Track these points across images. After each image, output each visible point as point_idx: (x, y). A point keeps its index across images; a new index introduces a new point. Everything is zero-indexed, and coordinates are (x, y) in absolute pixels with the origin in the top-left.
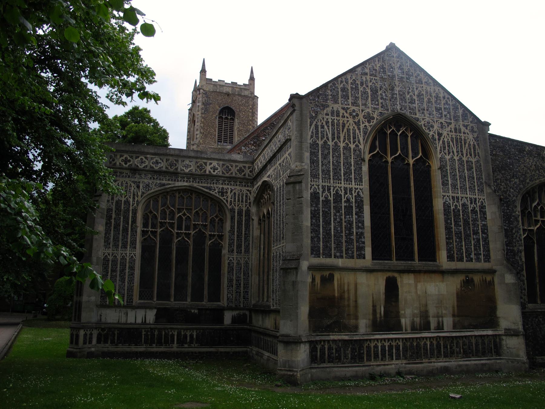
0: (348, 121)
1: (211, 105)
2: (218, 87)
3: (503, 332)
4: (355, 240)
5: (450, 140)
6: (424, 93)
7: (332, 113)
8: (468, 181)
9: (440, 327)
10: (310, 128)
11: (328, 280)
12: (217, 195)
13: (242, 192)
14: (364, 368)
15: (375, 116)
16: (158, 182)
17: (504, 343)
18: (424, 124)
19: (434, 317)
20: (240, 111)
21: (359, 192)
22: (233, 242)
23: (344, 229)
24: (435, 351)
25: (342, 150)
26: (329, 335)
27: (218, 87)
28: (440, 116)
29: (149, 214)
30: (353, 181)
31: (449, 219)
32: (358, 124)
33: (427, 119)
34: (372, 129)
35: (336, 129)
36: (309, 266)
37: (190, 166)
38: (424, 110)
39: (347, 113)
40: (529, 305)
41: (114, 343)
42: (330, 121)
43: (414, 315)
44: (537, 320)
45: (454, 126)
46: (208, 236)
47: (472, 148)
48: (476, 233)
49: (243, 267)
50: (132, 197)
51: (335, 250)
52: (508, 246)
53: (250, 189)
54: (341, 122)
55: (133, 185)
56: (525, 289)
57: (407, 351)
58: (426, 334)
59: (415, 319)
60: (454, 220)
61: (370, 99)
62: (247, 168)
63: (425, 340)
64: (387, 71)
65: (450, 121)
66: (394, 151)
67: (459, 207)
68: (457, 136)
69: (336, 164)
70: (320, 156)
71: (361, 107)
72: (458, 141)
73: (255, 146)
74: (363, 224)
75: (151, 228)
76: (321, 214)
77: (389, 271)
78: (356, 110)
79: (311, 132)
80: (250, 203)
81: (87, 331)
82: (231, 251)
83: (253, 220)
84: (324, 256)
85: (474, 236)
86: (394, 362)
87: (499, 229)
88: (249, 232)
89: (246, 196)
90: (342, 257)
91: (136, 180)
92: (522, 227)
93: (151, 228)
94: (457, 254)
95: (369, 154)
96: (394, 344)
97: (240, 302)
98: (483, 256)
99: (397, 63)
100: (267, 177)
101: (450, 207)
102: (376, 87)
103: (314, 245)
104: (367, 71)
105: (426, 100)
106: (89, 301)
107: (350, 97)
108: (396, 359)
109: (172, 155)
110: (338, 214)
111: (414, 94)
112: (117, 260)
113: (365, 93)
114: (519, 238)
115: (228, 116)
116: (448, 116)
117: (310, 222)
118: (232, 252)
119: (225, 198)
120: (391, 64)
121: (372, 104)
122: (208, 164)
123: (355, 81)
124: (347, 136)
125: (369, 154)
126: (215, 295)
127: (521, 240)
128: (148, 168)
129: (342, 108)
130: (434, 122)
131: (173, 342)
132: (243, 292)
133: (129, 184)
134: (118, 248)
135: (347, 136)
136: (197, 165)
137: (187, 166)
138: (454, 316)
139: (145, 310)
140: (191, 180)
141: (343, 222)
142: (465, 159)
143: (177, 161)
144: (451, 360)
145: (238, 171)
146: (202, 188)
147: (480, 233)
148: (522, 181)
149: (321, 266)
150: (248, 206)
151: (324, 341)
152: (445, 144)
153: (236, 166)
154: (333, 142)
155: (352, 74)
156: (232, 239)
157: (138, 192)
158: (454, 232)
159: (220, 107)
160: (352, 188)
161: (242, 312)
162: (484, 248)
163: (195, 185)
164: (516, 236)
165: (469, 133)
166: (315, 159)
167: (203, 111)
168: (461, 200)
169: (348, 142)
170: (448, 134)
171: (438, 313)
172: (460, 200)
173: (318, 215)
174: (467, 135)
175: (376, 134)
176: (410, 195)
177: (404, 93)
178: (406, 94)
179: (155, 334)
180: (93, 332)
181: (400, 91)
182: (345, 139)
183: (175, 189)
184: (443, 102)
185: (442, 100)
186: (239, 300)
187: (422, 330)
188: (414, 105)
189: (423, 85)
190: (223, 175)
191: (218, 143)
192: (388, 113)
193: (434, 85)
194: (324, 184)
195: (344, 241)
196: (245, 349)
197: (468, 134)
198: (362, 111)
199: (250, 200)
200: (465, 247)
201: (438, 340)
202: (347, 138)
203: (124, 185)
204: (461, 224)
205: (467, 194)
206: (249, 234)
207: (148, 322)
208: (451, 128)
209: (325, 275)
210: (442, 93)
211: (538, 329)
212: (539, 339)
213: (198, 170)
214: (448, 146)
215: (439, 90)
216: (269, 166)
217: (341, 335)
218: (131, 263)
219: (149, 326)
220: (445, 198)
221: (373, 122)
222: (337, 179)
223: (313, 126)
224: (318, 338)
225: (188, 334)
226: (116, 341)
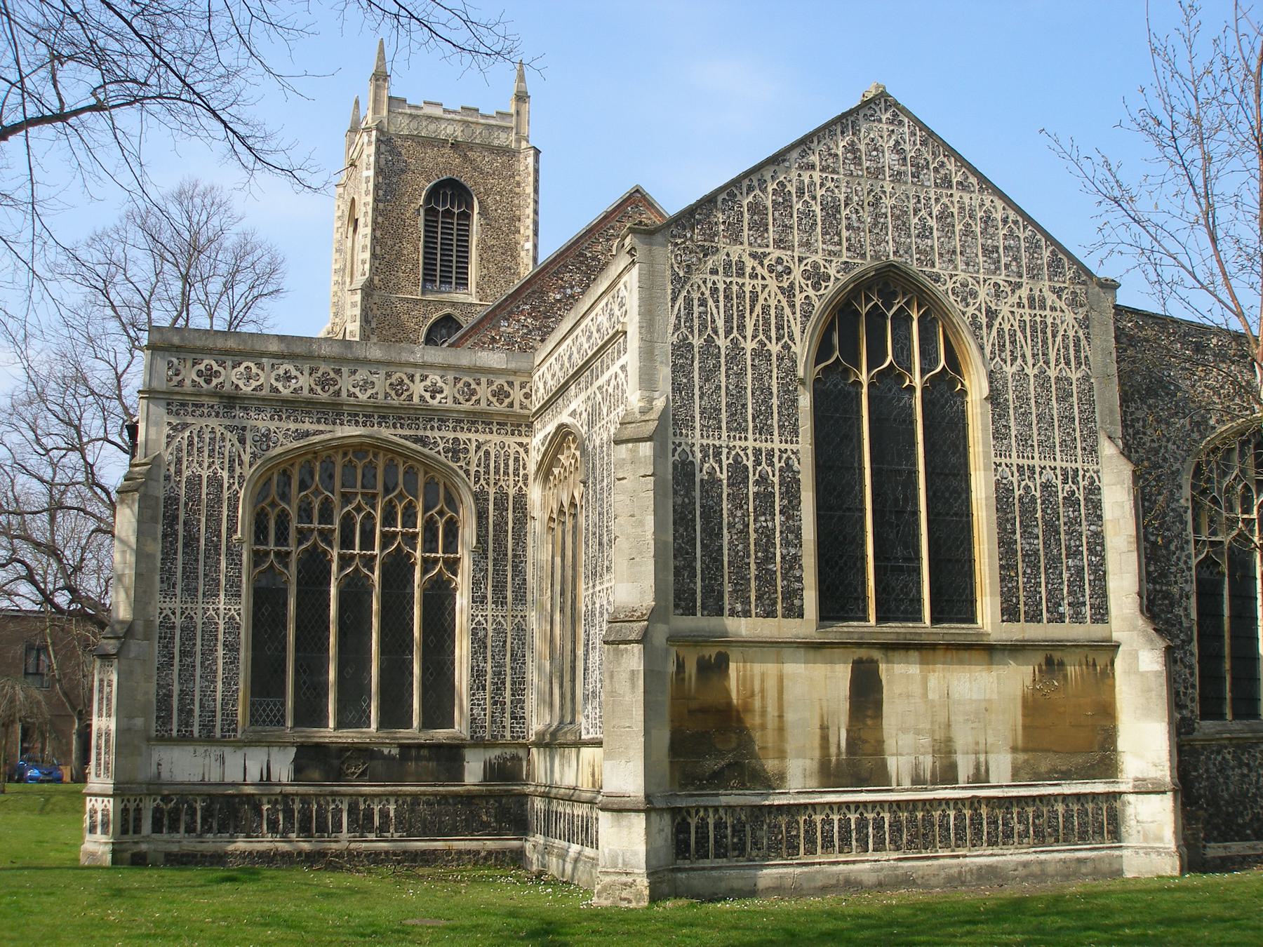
0: (764, 287)
3: (1131, 785)
4: (779, 574)
5: (1016, 327)
6: (955, 211)
7: (728, 265)
8: (1060, 426)
9: (980, 777)
11: (715, 668)
12: (442, 458)
13: (506, 448)
14: (799, 870)
15: (832, 272)
16: (293, 426)
17: (1130, 811)
20: (487, 193)
21: (789, 458)
23: (752, 547)
24: (968, 831)
25: (748, 356)
26: (717, 795)
28: (993, 267)
29: (269, 509)
30: (776, 433)
31: (1007, 520)
32: (789, 292)
33: (962, 276)
35: (735, 308)
36: (671, 636)
38: (954, 252)
39: (762, 266)
40: (1203, 723)
41: (194, 830)
42: (721, 286)
43: (917, 751)
44: (1219, 758)
45: (1028, 292)
47: (1072, 345)
48: (1074, 553)
49: (509, 640)
52: (1158, 583)
54: (748, 289)
55: (228, 435)
56: (1193, 686)
57: (900, 830)
58: (947, 791)
60: (1021, 522)
61: (819, 229)
63: (944, 806)
65: (1018, 280)
66: (876, 356)
67: (1033, 493)
68: (1035, 315)
69: (734, 392)
72: (1039, 331)
73: (535, 318)
74: (798, 536)
75: (276, 545)
76: (698, 513)
77: (859, 645)
78: (785, 258)
79: (674, 317)
80: (526, 477)
81: (128, 801)
82: (478, 600)
85: (1070, 561)
86: (870, 856)
87: (1129, 543)
89: (516, 460)
90: (747, 614)
91: (236, 422)
92: (1192, 535)
93: (276, 545)
94: (1025, 604)
95: (816, 364)
97: (504, 727)
98: (1091, 608)
99: (890, 135)
100: (570, 415)
101: (1013, 490)
102: (834, 198)
103: (682, 586)
104: (815, 159)
105: (959, 227)
106: (129, 729)
107: (771, 228)
110: (739, 513)
111: (930, 214)
112: (195, 627)
114: (1186, 562)
115: (452, 205)
116: (1014, 267)
117: (671, 532)
118: (482, 602)
122: (417, 378)
124: (761, 322)
125: (816, 364)
126: (438, 711)
127: (1190, 569)
128: (265, 392)
129: (750, 255)
130: (978, 282)
133: (219, 435)
134: (196, 596)
135: (761, 322)
138: (1014, 749)
139: (266, 749)
141: (751, 531)
142: (1052, 373)
146: (403, 441)
147: (1085, 553)
148: (1198, 424)
149: (699, 636)
150: (521, 484)
151: (706, 808)
152: (1003, 337)
154: (729, 340)
155: (776, 168)
157: (242, 453)
158: (1019, 553)
160: (773, 450)
161: (509, 752)
162: (1094, 590)
164: (1179, 559)
165: (1064, 307)
166: (685, 380)
167: (381, 193)
168: (1041, 473)
169: (764, 339)
170: (1012, 313)
172: (1037, 476)
174: (1061, 314)
175: (832, 322)
176: (915, 464)
179: (293, 809)
180: (141, 805)
181: (895, 207)
182: (756, 330)
183: (334, 443)
184: (1002, 233)
185: (1000, 226)
188: (929, 242)
189: (954, 191)
191: (424, 286)
192: (865, 264)
193: (981, 190)
194: (705, 442)
195: (752, 576)
197: (1063, 311)
199: (524, 469)
200: (1046, 586)
201: (976, 805)
202: (761, 328)
203: (207, 437)
204: (1039, 531)
205: (1055, 459)
207: (274, 779)
208: (1020, 297)
209: (707, 657)
210: (1000, 208)
211: (1221, 780)
212: (1222, 803)
214: (1010, 342)
215: (992, 201)
216: (573, 387)
217: (745, 795)
219: (278, 789)
220: (1000, 469)
221: (826, 287)
222: (736, 429)
223: (680, 301)
224: (692, 802)
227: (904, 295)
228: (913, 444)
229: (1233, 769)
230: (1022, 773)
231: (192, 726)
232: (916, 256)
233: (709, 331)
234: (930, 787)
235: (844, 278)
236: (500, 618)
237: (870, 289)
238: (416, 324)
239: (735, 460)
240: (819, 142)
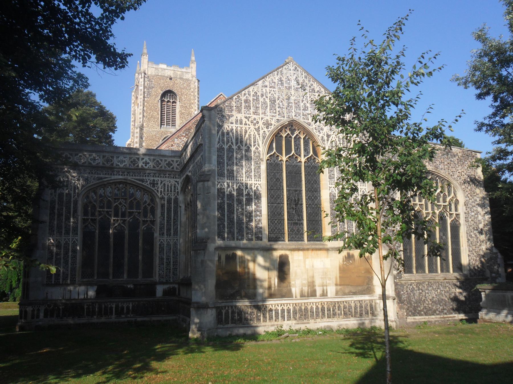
0: (249, 128)
1: (153, 89)
2: (160, 70)
7: (237, 121)
9: (324, 294)
10: (217, 135)
12: (149, 186)
15: (273, 122)
16: (96, 176)
18: (315, 128)
19: (319, 286)
20: (182, 95)
21: (257, 186)
22: (164, 227)
26: (232, 302)
27: (160, 70)
32: (258, 130)
34: (270, 134)
37: (125, 161)
40: (405, 275)
43: (303, 285)
44: (411, 287)
46: (141, 222)
50: (73, 190)
51: (237, 234)
53: (178, 180)
54: (244, 129)
57: (296, 313)
59: (304, 288)
62: (175, 162)
64: (284, 83)
66: (288, 151)
70: (225, 158)
71: (261, 116)
78: (256, 118)
80: (178, 192)
83: (180, 207)
84: (228, 239)
88: (177, 217)
89: (175, 187)
93: (91, 216)
96: (286, 308)
104: (267, 83)
108: (288, 320)
109: (108, 152)
110: (240, 205)
111: (308, 102)
112: (61, 245)
113: (265, 103)
118: (163, 235)
119: (156, 188)
120: (288, 77)
121: (270, 113)
123: (257, 93)
126: (149, 271)
131: (111, 313)
132: (173, 269)
136: (131, 160)
137: (122, 162)
138: (336, 285)
140: (126, 174)
143: (113, 157)
144: (333, 320)
145: (167, 164)
146: (135, 181)
150: (176, 195)
153: (166, 161)
155: (254, 87)
156: (162, 224)
159: (162, 91)
160: (252, 184)
161: (171, 286)
163: (129, 178)
166: (222, 161)
171: (323, 283)
173: (223, 207)
177: (299, 101)
178: (301, 102)
183: (111, 182)
186: (169, 276)
187: (309, 297)
190: (154, 169)
192: (285, 120)
196: (174, 317)
198: (262, 119)
199: (177, 189)
201: (323, 304)
206: (178, 219)
211: (412, 295)
213: (132, 165)
218: (74, 247)
224: (223, 304)
225: (125, 306)
226: (61, 315)
227: (298, 130)
228: (301, 181)
229: (416, 291)
230: (339, 293)
231: (59, 279)
232: (302, 117)
233: (230, 143)
234: (306, 298)
235: (276, 124)
236: (169, 240)
237: (286, 128)
238: (158, 139)
239: (239, 187)
240: (269, 78)
